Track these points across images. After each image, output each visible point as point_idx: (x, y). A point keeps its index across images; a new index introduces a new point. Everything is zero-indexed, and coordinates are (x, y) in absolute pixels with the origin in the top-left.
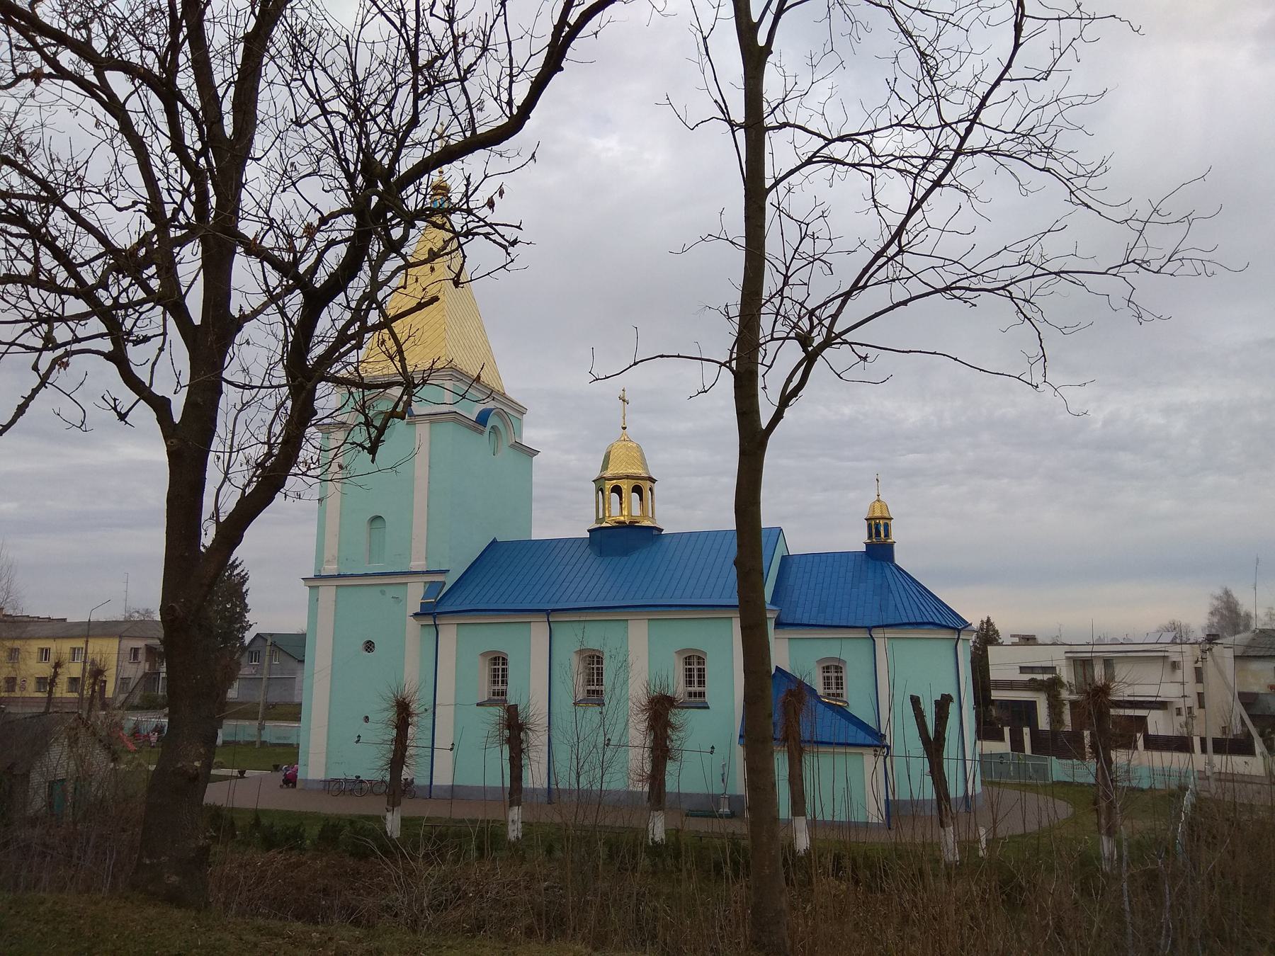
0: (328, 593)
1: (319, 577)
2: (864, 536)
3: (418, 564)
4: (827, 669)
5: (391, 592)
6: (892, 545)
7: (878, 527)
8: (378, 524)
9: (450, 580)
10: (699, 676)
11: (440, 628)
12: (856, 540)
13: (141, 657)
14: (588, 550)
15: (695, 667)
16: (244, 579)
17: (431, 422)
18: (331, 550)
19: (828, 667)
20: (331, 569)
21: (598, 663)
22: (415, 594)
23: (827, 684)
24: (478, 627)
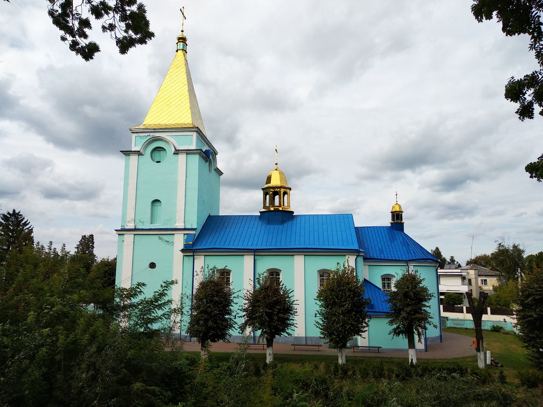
0: (129, 238)
1: (122, 230)
2: (390, 221)
3: (181, 225)
4: (383, 279)
5: (165, 238)
6: (403, 223)
7: (397, 216)
8: (157, 204)
9: (197, 233)
10: (385, 286)
11: (195, 257)
12: (387, 221)
13: (318, 315)
14: (260, 223)
15: (386, 282)
16: (31, 231)
17: (187, 154)
18: (130, 215)
19: (384, 279)
20: (131, 226)
21: (277, 275)
22: (179, 241)
23: (384, 285)
24: (373, 267)
